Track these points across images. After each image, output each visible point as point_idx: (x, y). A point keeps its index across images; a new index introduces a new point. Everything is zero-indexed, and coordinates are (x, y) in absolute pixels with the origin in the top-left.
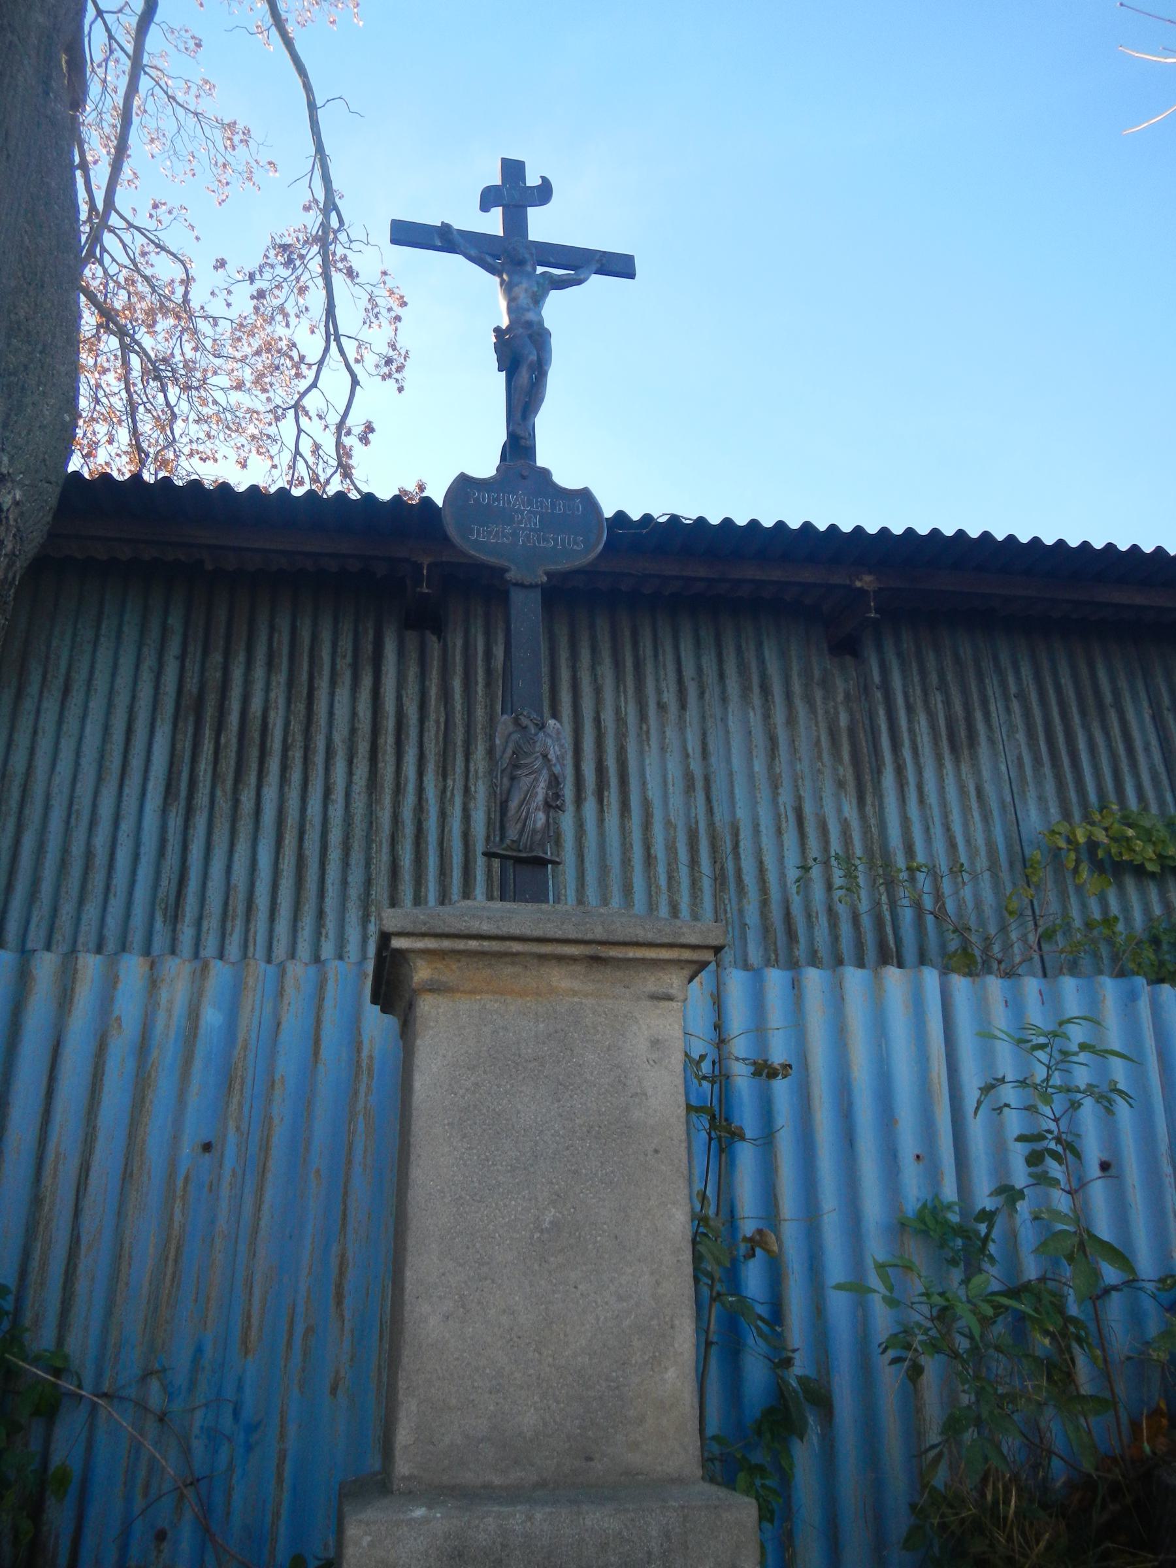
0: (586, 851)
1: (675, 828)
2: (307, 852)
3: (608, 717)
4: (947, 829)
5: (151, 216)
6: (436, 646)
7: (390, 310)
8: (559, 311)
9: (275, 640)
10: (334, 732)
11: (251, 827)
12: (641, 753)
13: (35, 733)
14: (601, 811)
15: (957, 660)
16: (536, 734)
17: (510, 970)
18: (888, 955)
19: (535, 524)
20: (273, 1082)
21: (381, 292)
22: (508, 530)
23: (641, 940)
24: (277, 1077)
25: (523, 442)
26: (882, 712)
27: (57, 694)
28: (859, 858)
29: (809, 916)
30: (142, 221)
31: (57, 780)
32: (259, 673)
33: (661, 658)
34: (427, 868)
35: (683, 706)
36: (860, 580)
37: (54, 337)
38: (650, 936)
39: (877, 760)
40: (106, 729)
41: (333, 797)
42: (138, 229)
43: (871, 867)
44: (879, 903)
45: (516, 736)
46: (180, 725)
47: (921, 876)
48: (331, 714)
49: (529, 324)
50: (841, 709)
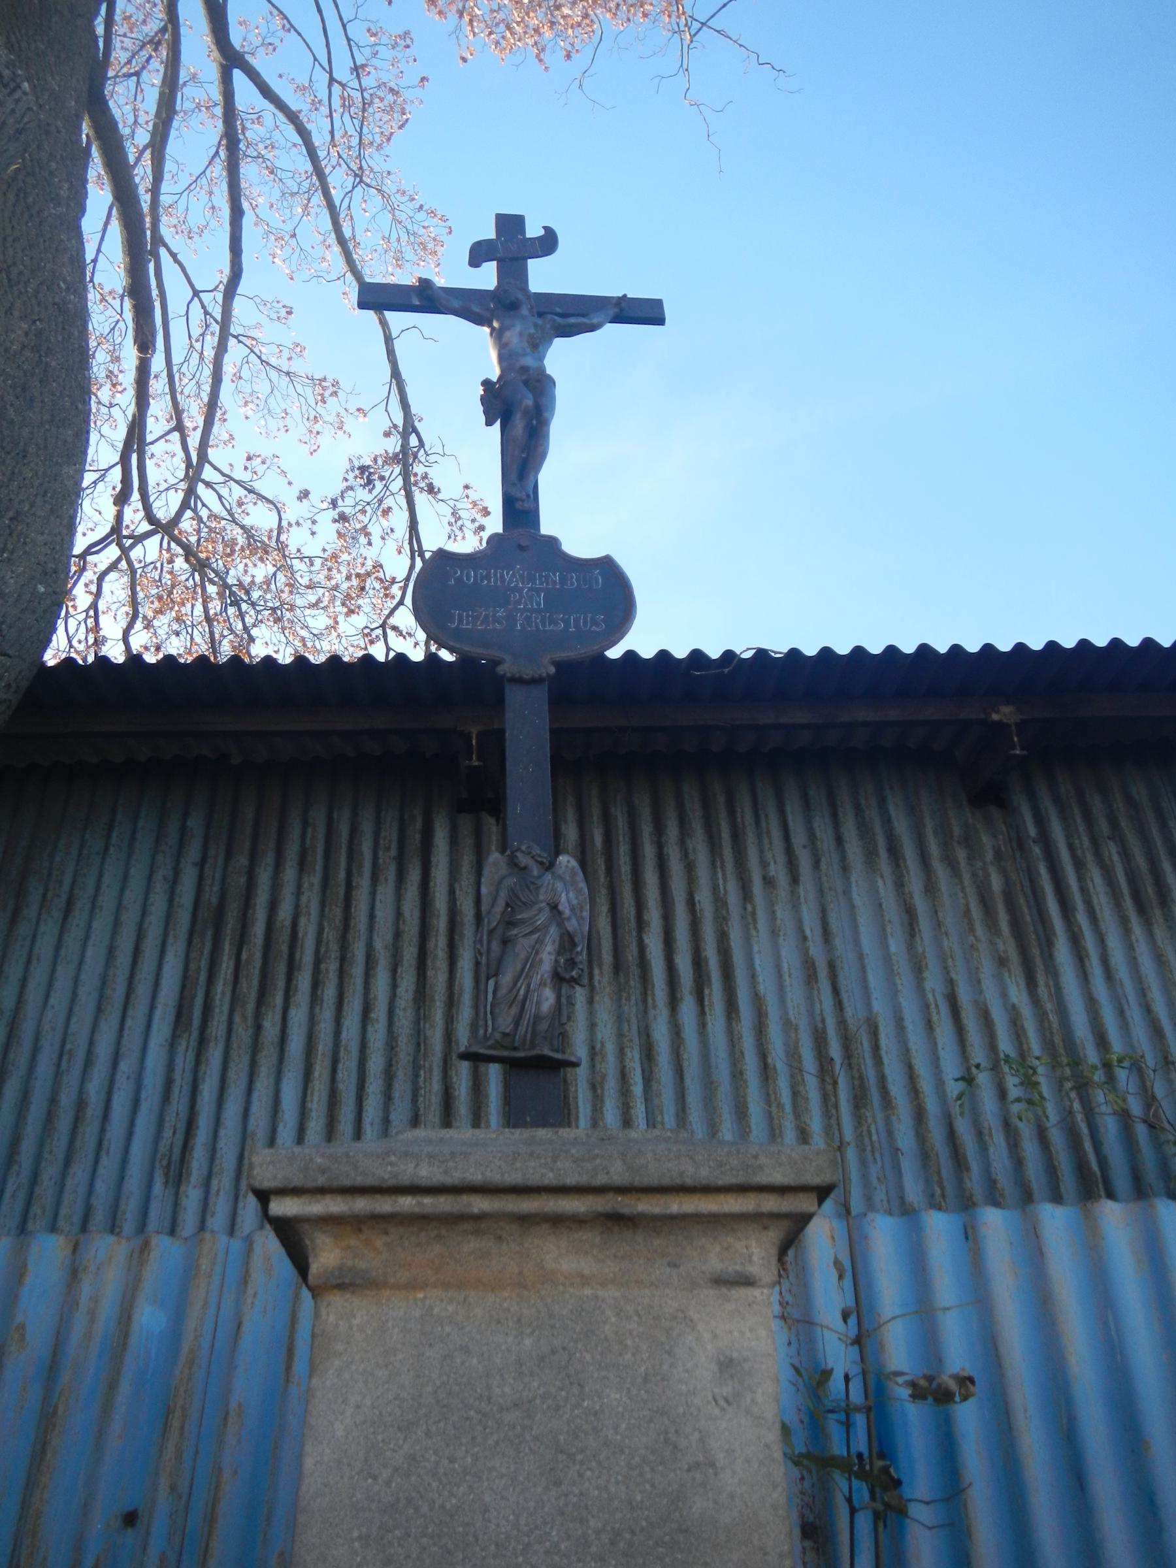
0: (685, 1064)
1: (796, 1029)
2: (341, 1086)
3: (704, 898)
4: (1148, 1010)
5: (246, 468)
6: (494, 829)
7: (473, 521)
8: (563, 358)
9: (309, 835)
10: (375, 937)
11: (274, 1058)
12: (747, 940)
13: (29, 961)
14: (702, 1013)
15: (1129, 800)
16: (539, 877)
17: (472, 1244)
18: (1092, 1186)
19: (538, 604)
20: (227, 1413)
21: (465, 504)
22: (501, 613)
23: (689, 1181)
24: (233, 1405)
25: (518, 505)
26: (1043, 871)
27: (57, 915)
28: (1038, 1058)
29: (980, 1134)
30: (239, 474)
31: (49, 1014)
32: (290, 874)
33: (763, 824)
34: (487, 1096)
35: (795, 879)
36: (998, 712)
37: (32, 505)
38: (705, 1175)
39: (1045, 930)
40: (111, 951)
41: (373, 1015)
42: (237, 482)
43: (1055, 1065)
44: (1071, 1112)
45: (511, 881)
46: (196, 940)
47: (1122, 1075)
48: (372, 916)
49: (525, 369)
50: (992, 870)
